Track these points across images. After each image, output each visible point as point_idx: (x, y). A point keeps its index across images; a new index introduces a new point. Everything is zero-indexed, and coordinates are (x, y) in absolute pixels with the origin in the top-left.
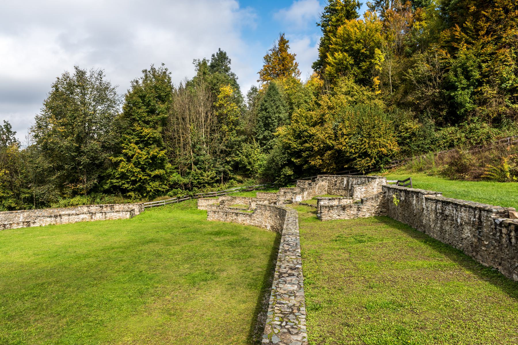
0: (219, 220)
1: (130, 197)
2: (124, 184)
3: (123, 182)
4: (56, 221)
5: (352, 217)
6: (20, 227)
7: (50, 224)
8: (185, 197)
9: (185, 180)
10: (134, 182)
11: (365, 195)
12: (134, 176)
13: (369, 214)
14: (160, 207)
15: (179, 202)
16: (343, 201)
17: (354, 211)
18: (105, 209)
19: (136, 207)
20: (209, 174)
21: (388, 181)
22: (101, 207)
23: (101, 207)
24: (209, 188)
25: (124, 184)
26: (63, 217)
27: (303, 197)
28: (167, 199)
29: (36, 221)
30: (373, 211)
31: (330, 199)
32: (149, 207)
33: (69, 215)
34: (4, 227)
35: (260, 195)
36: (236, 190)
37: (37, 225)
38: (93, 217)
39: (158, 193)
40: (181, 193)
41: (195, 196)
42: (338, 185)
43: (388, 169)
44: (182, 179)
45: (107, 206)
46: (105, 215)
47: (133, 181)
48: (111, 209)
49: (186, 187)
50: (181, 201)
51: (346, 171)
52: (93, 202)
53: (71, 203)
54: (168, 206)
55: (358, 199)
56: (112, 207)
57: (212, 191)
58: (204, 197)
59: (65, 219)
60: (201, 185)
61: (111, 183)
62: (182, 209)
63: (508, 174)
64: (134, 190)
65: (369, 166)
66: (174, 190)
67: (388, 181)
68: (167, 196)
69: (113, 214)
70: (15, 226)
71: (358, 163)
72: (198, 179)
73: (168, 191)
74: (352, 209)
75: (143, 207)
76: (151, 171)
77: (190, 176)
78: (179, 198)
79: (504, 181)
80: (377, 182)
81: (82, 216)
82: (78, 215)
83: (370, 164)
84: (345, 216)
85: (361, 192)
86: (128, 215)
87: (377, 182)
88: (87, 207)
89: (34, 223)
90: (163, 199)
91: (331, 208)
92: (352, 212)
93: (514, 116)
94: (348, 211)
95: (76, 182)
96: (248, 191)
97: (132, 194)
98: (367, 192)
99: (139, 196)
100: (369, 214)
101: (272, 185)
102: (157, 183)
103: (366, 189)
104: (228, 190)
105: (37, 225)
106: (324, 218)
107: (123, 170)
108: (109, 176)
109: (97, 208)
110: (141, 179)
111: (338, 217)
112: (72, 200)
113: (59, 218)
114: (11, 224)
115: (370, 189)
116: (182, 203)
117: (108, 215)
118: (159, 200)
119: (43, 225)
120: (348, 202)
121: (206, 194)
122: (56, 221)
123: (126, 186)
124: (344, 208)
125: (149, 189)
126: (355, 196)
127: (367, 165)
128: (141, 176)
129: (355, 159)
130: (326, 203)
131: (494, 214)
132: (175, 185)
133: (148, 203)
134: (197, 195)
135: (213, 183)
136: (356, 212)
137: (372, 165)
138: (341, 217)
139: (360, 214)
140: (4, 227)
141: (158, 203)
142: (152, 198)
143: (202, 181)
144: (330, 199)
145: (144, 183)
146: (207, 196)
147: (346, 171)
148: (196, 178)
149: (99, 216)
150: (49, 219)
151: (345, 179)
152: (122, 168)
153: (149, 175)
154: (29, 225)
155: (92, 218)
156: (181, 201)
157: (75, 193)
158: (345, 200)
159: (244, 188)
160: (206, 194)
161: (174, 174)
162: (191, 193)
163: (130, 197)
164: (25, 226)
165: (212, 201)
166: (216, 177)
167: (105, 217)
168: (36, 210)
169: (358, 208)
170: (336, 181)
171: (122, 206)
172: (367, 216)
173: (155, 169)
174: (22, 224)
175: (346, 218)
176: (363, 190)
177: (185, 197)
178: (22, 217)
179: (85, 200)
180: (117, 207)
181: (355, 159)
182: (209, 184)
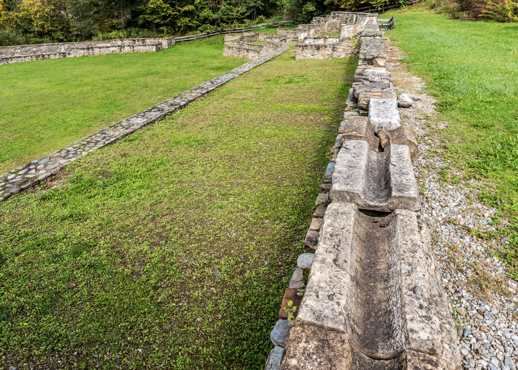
0: (233, 56)
1: (162, 32)
2: (156, 19)
3: (155, 17)
4: (88, 53)
5: (327, 57)
6: (57, 57)
7: (84, 56)
8: (214, 33)
9: (215, 16)
10: (165, 18)
12: (163, 12)
13: (345, 55)
14: (190, 42)
15: (209, 37)
16: (328, 40)
17: (329, 51)
18: (137, 43)
19: (165, 43)
20: (239, 9)
21: (378, 20)
22: (133, 40)
24: (236, 24)
25: (156, 19)
26: (95, 49)
28: (197, 34)
29: (71, 52)
30: (349, 51)
31: (315, 38)
32: (181, 42)
33: (100, 48)
34: (43, 57)
35: (280, 31)
37: (72, 56)
39: (189, 28)
41: (223, 31)
43: (408, 5)
44: (212, 14)
46: (133, 48)
47: (163, 16)
48: (143, 43)
49: (213, 22)
50: (211, 36)
51: (367, 7)
52: (128, 36)
53: (109, 37)
54: (198, 40)
56: (143, 41)
57: (239, 27)
58: (232, 33)
59: (96, 51)
60: (230, 21)
61: (145, 19)
62: (210, 44)
63: (510, 14)
64: (166, 25)
66: (204, 26)
67: (378, 20)
68: (198, 32)
69: (140, 48)
70: (52, 57)
72: (228, 14)
73: (198, 26)
74: (327, 49)
75: (174, 41)
76: (181, 7)
77: (220, 12)
78: (208, 33)
79: (504, 22)
80: (367, 21)
81: (112, 49)
82: (108, 47)
84: (319, 56)
85: (348, 31)
87: (367, 21)
88: (121, 40)
89: (69, 54)
90: (193, 34)
91: (305, 48)
92: (327, 52)
94: (323, 50)
95: (112, 18)
96: (274, 27)
97: (164, 28)
99: (171, 30)
100: (345, 55)
101: (297, 21)
102: (187, 19)
103: (355, 27)
104: (255, 26)
105: (72, 56)
106: (298, 57)
107: (153, 6)
108: (142, 12)
109: (130, 41)
110: (170, 15)
111: (312, 57)
112: (110, 34)
113: (91, 51)
114: (49, 55)
116: (211, 38)
117: (135, 48)
118: (190, 35)
119: (78, 56)
120: (334, 42)
122: (88, 53)
123: (158, 21)
124: (318, 48)
125: (179, 24)
128: (171, 12)
130: (312, 42)
131: (361, 61)
132: (205, 20)
134: (225, 31)
135: (244, 18)
136: (331, 52)
138: (315, 57)
139: (335, 55)
140: (43, 57)
141: (189, 38)
142: (184, 33)
143: (231, 17)
144: (315, 38)
145: (175, 19)
146: (234, 32)
147: (367, 7)
148: (226, 13)
149: (127, 49)
150: (82, 51)
151: (355, 16)
152: (152, 4)
153: (179, 11)
154: (65, 56)
155: (121, 51)
156: (211, 36)
157: (113, 27)
158: (331, 39)
159: (270, 24)
161: (205, 10)
162: (219, 29)
163: (162, 32)
164: (61, 57)
165: (237, 37)
166: (246, 12)
167: (134, 51)
168: (75, 43)
169: (333, 48)
170: (347, 19)
171: (152, 40)
172: (342, 57)
173: (185, 5)
174: (58, 55)
175: (320, 58)
176: (351, 29)
177: (214, 33)
178: (63, 49)
179: (121, 34)
180: (148, 41)
182: (238, 19)
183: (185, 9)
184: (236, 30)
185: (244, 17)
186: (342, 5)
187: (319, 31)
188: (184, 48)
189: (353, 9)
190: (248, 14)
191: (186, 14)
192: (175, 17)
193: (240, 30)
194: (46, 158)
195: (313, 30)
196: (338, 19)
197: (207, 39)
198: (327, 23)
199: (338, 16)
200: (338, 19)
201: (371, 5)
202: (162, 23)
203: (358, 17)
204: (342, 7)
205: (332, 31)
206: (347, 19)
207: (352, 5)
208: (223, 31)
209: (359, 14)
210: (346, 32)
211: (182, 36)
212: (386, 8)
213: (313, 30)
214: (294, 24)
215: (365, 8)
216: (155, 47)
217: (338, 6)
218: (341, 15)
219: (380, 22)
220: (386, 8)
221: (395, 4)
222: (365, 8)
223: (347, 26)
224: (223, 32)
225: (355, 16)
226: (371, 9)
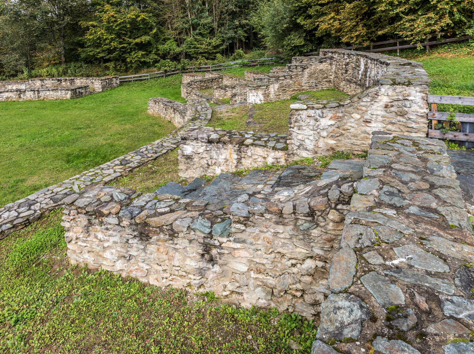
2: (99, 53)
8: (174, 71)
10: (110, 51)
11: (332, 142)
13: (259, 292)
18: (64, 83)
21: (432, 99)
22: (59, 80)
23: (59, 80)
24: (202, 60)
25: (99, 53)
27: (266, 95)
31: (210, 142)
32: (130, 81)
36: (235, 64)
38: (22, 96)
39: (143, 65)
40: (169, 64)
41: (184, 69)
42: (350, 71)
45: (66, 79)
46: (39, 93)
50: (169, 75)
51: (392, 41)
54: (152, 80)
55: (305, 154)
57: (206, 64)
65: (433, 32)
69: (48, 93)
71: (408, 25)
73: (156, 61)
78: (166, 71)
80: (384, 100)
83: (436, 28)
86: (69, 96)
88: (41, 80)
90: (147, 73)
93: (473, 42)
96: (250, 66)
98: (338, 132)
102: (140, 53)
103: (339, 119)
115: (353, 122)
116: (170, 78)
117: (42, 94)
118: (144, 73)
120: (270, 161)
121: (199, 69)
123: (101, 55)
126: (294, 142)
127: (428, 30)
129: (397, 18)
133: (124, 77)
137: (442, 30)
141: (125, 79)
142: (137, 70)
147: (392, 41)
148: (192, 46)
155: (20, 97)
156: (169, 75)
158: (259, 151)
160: (199, 69)
170: (347, 64)
176: (325, 122)
177: (174, 71)
181: (397, 18)
183: (138, 40)
184: (201, 68)
185: (218, 50)
186: (343, 36)
187: (289, 86)
188: (122, 94)
189: (366, 44)
190: (224, 47)
191: (141, 46)
192: (124, 51)
193: (207, 68)
194: (264, 86)
195: (277, 86)
196: (331, 64)
197: (164, 79)
198: (307, 71)
199: (331, 58)
200: (331, 64)
201: (400, 37)
202: (107, 57)
203: (370, 65)
204: (344, 40)
205: (320, 87)
206: (347, 64)
207: (363, 36)
208: (184, 69)
209: (372, 59)
210: (308, 132)
211: (135, 74)
212: (434, 42)
213: (277, 86)
214: (277, 62)
215: (388, 42)
216: (70, 92)
217: (338, 38)
218: (336, 56)
219: (442, 109)
220: (434, 42)
221: (454, 35)
222: (388, 42)
223: (311, 112)
224: (184, 70)
225: (362, 61)
226: (401, 43)
